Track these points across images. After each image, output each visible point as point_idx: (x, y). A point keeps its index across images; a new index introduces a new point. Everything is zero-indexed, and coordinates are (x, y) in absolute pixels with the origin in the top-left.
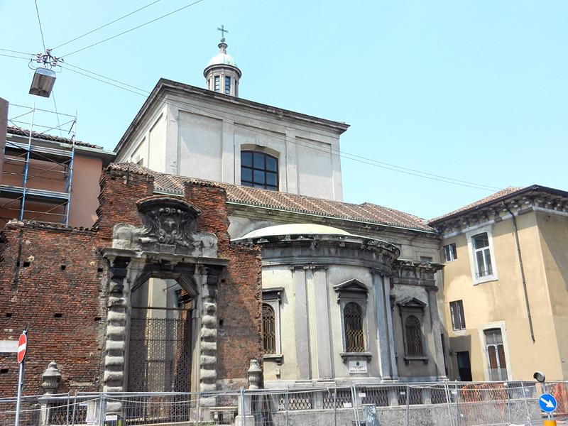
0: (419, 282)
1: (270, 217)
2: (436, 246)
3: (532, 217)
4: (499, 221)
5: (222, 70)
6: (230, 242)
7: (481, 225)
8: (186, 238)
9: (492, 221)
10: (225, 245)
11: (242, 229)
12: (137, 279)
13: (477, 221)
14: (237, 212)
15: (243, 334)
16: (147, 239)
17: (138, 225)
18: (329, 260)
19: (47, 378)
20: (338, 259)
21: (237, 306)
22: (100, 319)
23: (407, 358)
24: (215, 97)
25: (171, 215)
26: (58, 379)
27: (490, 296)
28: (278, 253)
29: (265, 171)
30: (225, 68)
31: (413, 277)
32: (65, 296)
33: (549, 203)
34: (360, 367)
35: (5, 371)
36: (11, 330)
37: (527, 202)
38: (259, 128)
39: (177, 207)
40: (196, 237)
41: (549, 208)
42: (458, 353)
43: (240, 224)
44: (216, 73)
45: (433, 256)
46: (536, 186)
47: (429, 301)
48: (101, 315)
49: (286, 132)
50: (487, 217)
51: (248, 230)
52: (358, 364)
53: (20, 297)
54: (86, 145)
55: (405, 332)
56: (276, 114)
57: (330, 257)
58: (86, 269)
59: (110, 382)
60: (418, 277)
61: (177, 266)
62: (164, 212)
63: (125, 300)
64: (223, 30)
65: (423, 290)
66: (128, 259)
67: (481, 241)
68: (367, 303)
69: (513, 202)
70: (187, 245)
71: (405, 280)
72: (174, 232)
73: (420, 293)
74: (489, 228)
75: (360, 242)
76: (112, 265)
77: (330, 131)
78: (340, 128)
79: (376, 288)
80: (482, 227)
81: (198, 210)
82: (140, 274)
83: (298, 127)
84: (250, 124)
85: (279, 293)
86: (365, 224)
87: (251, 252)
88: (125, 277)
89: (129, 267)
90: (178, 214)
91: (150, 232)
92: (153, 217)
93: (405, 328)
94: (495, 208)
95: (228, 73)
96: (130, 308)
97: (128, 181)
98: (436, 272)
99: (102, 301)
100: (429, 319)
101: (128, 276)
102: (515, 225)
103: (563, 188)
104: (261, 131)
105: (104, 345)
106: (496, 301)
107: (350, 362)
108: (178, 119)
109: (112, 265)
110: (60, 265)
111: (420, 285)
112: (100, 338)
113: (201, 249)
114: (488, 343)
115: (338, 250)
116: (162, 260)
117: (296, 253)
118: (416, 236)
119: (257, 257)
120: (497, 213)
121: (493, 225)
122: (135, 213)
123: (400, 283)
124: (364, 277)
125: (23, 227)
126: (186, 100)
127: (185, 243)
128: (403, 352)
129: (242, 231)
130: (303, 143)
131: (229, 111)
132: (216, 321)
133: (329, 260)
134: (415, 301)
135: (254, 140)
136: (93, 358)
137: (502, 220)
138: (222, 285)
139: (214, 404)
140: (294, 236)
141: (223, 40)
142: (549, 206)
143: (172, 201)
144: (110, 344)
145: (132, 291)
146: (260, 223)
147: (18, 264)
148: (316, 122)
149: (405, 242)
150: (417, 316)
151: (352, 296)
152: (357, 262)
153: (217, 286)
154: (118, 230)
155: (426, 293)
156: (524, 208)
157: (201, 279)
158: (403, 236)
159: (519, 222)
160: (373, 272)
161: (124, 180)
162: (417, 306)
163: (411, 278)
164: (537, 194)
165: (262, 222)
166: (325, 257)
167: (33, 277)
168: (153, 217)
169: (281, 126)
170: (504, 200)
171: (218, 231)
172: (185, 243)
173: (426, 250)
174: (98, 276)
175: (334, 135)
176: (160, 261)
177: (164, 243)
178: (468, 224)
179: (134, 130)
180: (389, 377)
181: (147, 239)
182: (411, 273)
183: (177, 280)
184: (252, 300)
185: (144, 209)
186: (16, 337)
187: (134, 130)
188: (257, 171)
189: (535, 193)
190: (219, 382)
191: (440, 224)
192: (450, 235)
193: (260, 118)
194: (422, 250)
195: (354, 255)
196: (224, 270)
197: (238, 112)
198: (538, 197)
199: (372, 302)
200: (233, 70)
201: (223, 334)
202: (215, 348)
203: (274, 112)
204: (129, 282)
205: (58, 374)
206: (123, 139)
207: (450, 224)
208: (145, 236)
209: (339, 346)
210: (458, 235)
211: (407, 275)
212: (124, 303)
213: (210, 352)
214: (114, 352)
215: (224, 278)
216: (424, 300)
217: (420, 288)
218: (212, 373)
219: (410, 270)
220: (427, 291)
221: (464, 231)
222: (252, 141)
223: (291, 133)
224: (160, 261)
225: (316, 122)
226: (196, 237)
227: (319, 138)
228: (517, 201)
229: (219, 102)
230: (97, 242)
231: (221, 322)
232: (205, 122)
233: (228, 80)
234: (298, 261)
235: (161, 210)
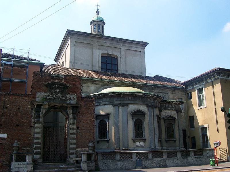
0: (174, 109)
1: (110, 84)
2: (184, 93)
3: (219, 80)
4: (207, 83)
5: (97, 22)
6: (82, 97)
7: (201, 84)
8: (64, 97)
9: (204, 83)
10: (80, 98)
11: (98, 90)
12: (46, 112)
13: (199, 83)
14: (96, 83)
15: (87, 132)
16: (49, 97)
17: (45, 92)
18: (129, 102)
19: (90, 146)
20: (132, 101)
21: (85, 121)
22: (32, 126)
23: (167, 140)
24: (90, 35)
25: (58, 88)
26: (18, 147)
27: (203, 114)
28: (108, 99)
29: (112, 64)
30: (98, 21)
31: (171, 107)
32: (20, 118)
33: (226, 75)
34: (141, 144)
35: (1, 144)
36: (2, 130)
37: (217, 75)
38: (109, 47)
39: (60, 85)
40: (68, 96)
41: (226, 77)
42: (192, 137)
43: (97, 87)
44: (94, 23)
45: (183, 98)
46: (219, 68)
47: (178, 117)
48: (32, 125)
49: (121, 47)
50: (203, 81)
51: (100, 90)
52: (140, 143)
53: (5, 119)
54: (36, 61)
55: (166, 130)
56: (116, 40)
57: (129, 101)
58: (27, 109)
59: (36, 148)
60: (173, 107)
61: (60, 107)
62: (55, 87)
63: (41, 120)
64: (97, 6)
65: (175, 112)
66: (42, 105)
67: (200, 91)
68: (145, 119)
69: (211, 75)
70: (64, 99)
71: (167, 108)
72: (59, 94)
73: (174, 114)
74: (203, 85)
75: (142, 94)
76: (36, 107)
77: (140, 46)
78: (145, 44)
79: (149, 112)
80: (201, 85)
81: (68, 86)
82: (46, 110)
83: (126, 45)
84: (105, 45)
85: (108, 116)
86: (151, 86)
87: (90, 101)
88: (41, 111)
89: (42, 108)
90: (61, 88)
91: (50, 95)
92: (51, 89)
93: (166, 127)
94: (205, 78)
95: (99, 23)
96: (43, 123)
97: (42, 76)
98: (181, 104)
99: (33, 121)
100: (177, 124)
101: (42, 111)
102: (213, 84)
103: (228, 68)
104: (110, 48)
105: (34, 135)
106: (205, 116)
107: (136, 142)
108: (75, 45)
109: (36, 107)
110: (18, 107)
111: (174, 110)
112: (32, 133)
113: (70, 100)
114: (202, 133)
115: (133, 98)
116: (54, 105)
117: (115, 99)
118: (175, 89)
119: (93, 103)
120: (206, 80)
121: (205, 85)
122: (44, 88)
123: (165, 110)
124: (144, 108)
125: (5, 94)
126: (78, 37)
127: (63, 98)
128: (165, 138)
129: (98, 90)
130: (128, 51)
131: (96, 40)
132: (76, 128)
133: (129, 102)
134: (171, 116)
135: (107, 51)
136: (30, 140)
137: (208, 83)
138: (78, 114)
139: (75, 157)
140: (114, 93)
141: (98, 9)
142: (226, 76)
143: (58, 83)
144: (36, 136)
145: (44, 116)
146: (105, 87)
147: (4, 107)
148: (134, 42)
149: (170, 92)
150: (172, 123)
151: (138, 116)
152: (141, 102)
153: (76, 114)
154: (38, 94)
155: (177, 113)
156: (216, 77)
157: (70, 111)
158: (169, 89)
159: (214, 83)
160: (148, 106)
161: (40, 75)
162: (173, 118)
163: (170, 108)
164: (220, 71)
165: (106, 86)
166: (127, 101)
167: (9, 112)
168: (51, 89)
169: (118, 45)
170: (208, 74)
171: (77, 93)
172: (63, 98)
173: (180, 95)
174: (31, 111)
175: (142, 47)
176: (54, 106)
177: (55, 98)
178: (196, 84)
179: (61, 49)
180: (160, 148)
181: (49, 97)
182: (170, 105)
183: (61, 112)
184: (91, 119)
185: (47, 86)
186: (4, 133)
187: (61, 49)
188: (108, 64)
189: (219, 71)
190: (77, 149)
191: (185, 84)
192: (190, 88)
193: (109, 42)
194: (178, 95)
195: (139, 100)
196: (79, 108)
197: (100, 41)
198: (221, 73)
199: (147, 118)
200: (101, 22)
201: (79, 132)
202: (35, 140)
203: (115, 39)
204: (42, 113)
205: (18, 145)
206: (58, 53)
207: (189, 84)
208: (48, 96)
209: (131, 134)
210: (192, 89)
211: (168, 106)
212: (41, 121)
213: (73, 139)
214: (37, 138)
215: (79, 111)
216: (176, 116)
217: (174, 111)
218: (74, 146)
219: (170, 104)
220: (177, 112)
221: (194, 87)
222: (106, 52)
223: (123, 48)
224: (54, 106)
225: (134, 42)
226: (68, 96)
227: (136, 49)
228: (213, 75)
229: (92, 37)
230: (30, 99)
231: (78, 128)
232: (86, 46)
233: (99, 26)
234: (116, 102)
235: (54, 86)
